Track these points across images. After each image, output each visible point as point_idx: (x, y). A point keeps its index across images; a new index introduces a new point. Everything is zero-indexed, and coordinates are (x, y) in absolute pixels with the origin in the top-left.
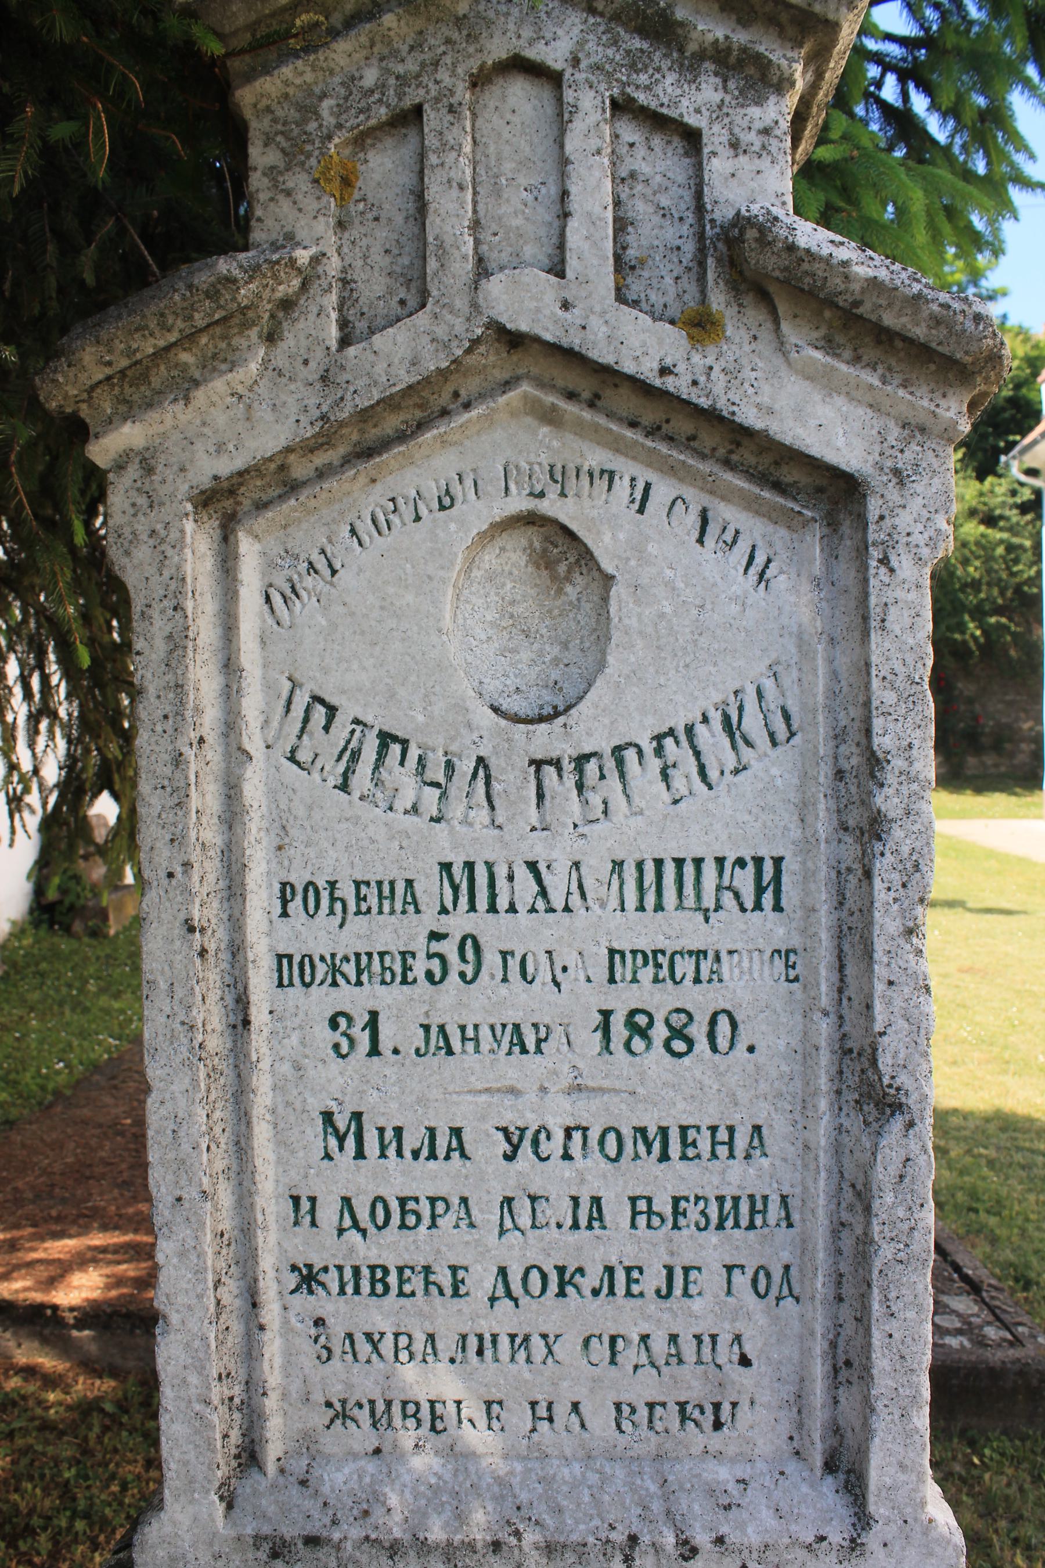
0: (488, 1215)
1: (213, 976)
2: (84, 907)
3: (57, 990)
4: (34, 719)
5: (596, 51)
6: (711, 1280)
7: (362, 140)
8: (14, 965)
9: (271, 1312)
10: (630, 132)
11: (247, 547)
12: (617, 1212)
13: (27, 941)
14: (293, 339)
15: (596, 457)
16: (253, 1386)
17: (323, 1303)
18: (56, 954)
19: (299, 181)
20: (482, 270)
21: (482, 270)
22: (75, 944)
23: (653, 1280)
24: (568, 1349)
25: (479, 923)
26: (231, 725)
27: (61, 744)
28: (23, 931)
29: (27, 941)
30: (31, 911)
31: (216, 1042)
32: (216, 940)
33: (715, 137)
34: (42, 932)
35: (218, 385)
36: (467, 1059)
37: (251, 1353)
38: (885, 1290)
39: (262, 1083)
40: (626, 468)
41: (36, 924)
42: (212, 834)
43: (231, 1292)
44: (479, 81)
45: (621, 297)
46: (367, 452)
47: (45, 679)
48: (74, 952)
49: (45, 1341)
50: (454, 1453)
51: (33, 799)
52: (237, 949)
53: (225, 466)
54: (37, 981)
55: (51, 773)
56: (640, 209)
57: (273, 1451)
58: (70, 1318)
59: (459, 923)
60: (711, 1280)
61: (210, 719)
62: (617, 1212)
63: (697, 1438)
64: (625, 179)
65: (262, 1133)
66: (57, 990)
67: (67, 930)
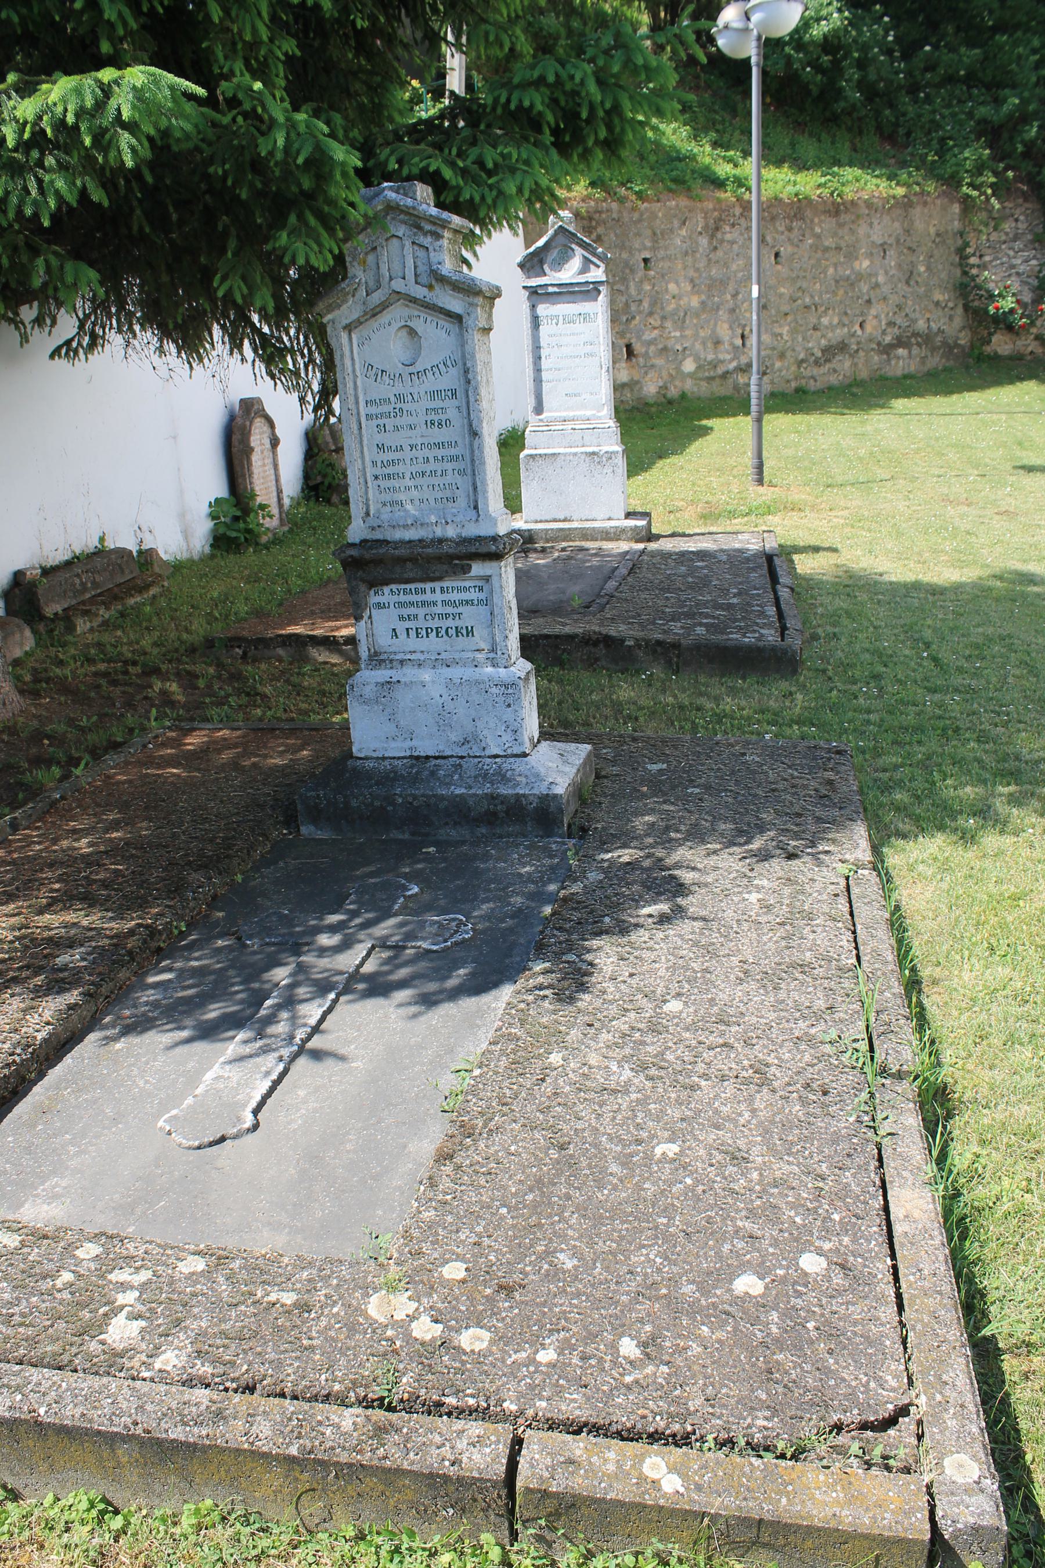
0: (408, 462)
1: (354, 419)
2: (338, 485)
3: (325, 536)
4: (306, 366)
5: (408, 233)
6: (450, 472)
7: (366, 254)
8: (296, 524)
9: (370, 484)
10: (416, 248)
11: (354, 336)
12: (432, 460)
13: (302, 510)
14: (357, 296)
15: (416, 313)
16: (367, 499)
17: (379, 482)
18: (321, 516)
19: (355, 264)
20: (391, 279)
21: (391, 279)
22: (334, 510)
23: (439, 473)
24: (425, 488)
25: (402, 405)
26: (354, 371)
27: (318, 375)
28: (299, 504)
29: (302, 510)
30: (303, 490)
31: (356, 432)
32: (355, 412)
33: (431, 249)
34: (312, 504)
35: (345, 306)
36: (402, 431)
37: (367, 493)
38: (586, 535)
39: (365, 442)
40: (422, 315)
41: (307, 498)
42: (352, 392)
43: (362, 480)
44: (387, 240)
45: (417, 283)
46: (374, 315)
47: (310, 350)
48: (335, 515)
49: (331, 651)
50: (405, 511)
51: (309, 398)
52: (358, 414)
53: (348, 322)
54: (312, 531)
55: (316, 387)
56: (419, 263)
57: (372, 513)
58: (341, 641)
59: (398, 406)
60: (450, 472)
61: (350, 370)
62: (432, 460)
63: (450, 504)
64: (415, 258)
65: (365, 449)
66: (325, 536)
67: (328, 501)
